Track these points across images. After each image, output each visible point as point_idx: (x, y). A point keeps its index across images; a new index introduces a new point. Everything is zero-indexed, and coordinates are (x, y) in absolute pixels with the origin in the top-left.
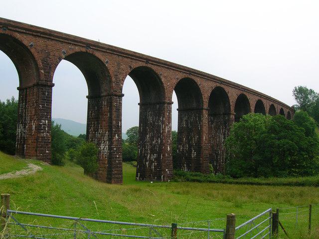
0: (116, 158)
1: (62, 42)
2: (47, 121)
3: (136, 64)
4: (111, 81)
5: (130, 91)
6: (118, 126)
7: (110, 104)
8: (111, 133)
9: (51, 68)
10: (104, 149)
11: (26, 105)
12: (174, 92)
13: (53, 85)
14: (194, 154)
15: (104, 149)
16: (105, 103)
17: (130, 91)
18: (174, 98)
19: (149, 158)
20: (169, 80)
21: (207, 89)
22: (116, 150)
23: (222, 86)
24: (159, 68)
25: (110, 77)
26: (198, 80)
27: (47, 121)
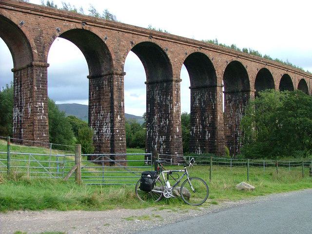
2: (43, 104)
5: (184, 79)
10: (106, 132)
11: (21, 87)
14: (208, 136)
15: (106, 132)
16: (106, 83)
20: (176, 56)
25: (109, 54)
27: (43, 104)
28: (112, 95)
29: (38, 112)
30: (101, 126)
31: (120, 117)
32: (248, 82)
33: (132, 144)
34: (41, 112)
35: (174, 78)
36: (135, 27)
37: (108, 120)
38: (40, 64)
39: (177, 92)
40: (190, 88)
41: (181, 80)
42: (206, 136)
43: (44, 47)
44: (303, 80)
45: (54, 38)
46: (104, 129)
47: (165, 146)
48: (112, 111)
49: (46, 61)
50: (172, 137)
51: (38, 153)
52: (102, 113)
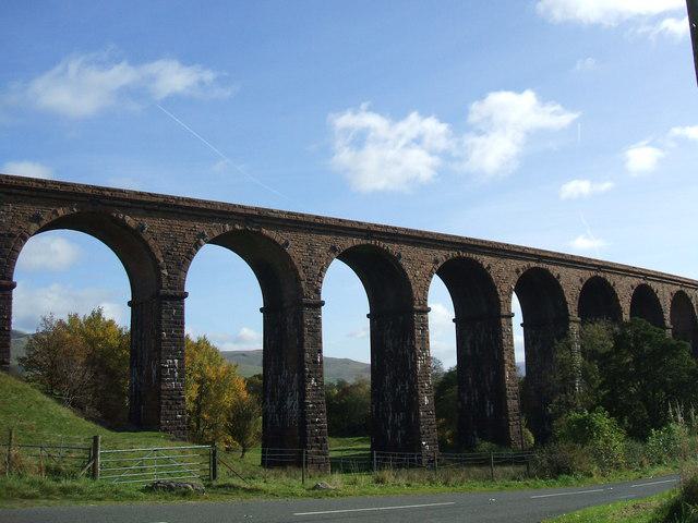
0: (313, 422)
1: (567, 266)
2: (176, 361)
3: (349, 243)
4: (298, 279)
5: (440, 310)
6: (316, 362)
7: (299, 324)
8: (304, 376)
9: (182, 262)
10: (292, 407)
11: (142, 332)
12: (514, 295)
13: (186, 295)
14: (490, 410)
15: (292, 407)
16: (290, 320)
17: (440, 310)
18: (515, 305)
19: (393, 421)
20: (505, 274)
21: (571, 284)
22: (313, 408)
23: (601, 275)
24: (655, 283)
25: (295, 271)
26: (555, 270)
27: (176, 361)
28: (302, 341)
29: (167, 376)
30: (283, 400)
31: (316, 381)
32: (565, 303)
33: (340, 429)
34: (174, 376)
35: (504, 312)
36: (340, 220)
37: (295, 384)
38: (172, 292)
39: (423, 330)
40: (261, 310)
41: (429, 310)
42: (487, 410)
43: (322, 268)
44: (680, 292)
45: (197, 246)
46: (289, 403)
47: (404, 432)
48: (301, 370)
49: (10, 279)
50: (417, 414)
51: (442, 501)
52: (286, 373)
